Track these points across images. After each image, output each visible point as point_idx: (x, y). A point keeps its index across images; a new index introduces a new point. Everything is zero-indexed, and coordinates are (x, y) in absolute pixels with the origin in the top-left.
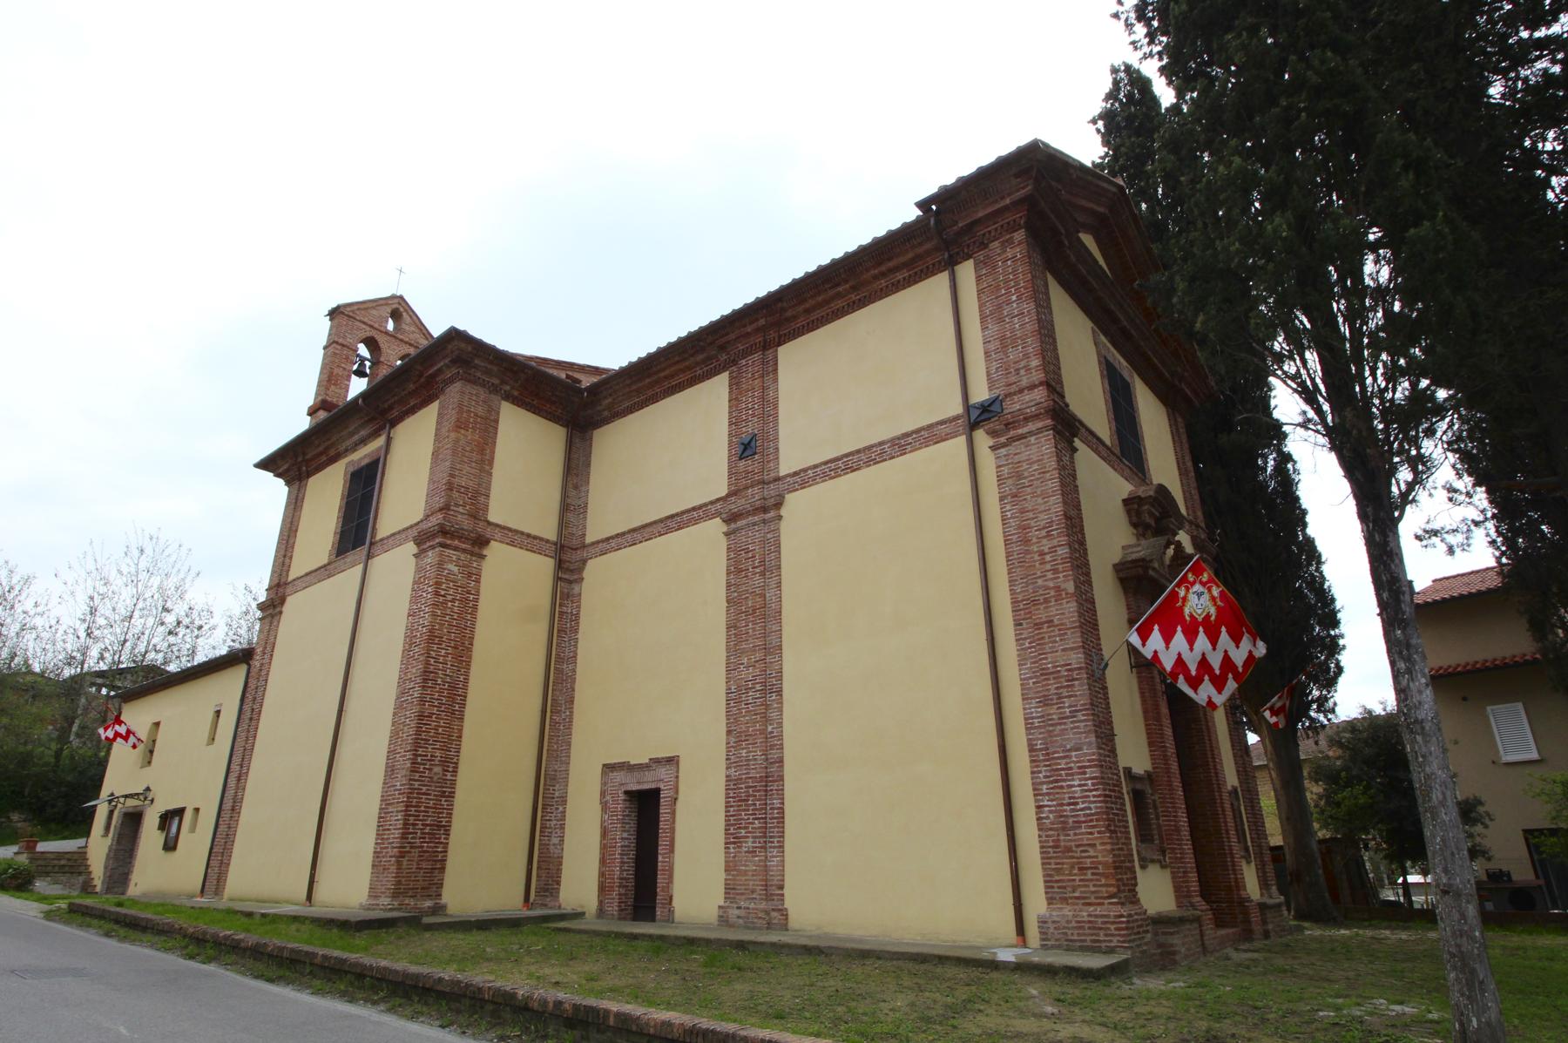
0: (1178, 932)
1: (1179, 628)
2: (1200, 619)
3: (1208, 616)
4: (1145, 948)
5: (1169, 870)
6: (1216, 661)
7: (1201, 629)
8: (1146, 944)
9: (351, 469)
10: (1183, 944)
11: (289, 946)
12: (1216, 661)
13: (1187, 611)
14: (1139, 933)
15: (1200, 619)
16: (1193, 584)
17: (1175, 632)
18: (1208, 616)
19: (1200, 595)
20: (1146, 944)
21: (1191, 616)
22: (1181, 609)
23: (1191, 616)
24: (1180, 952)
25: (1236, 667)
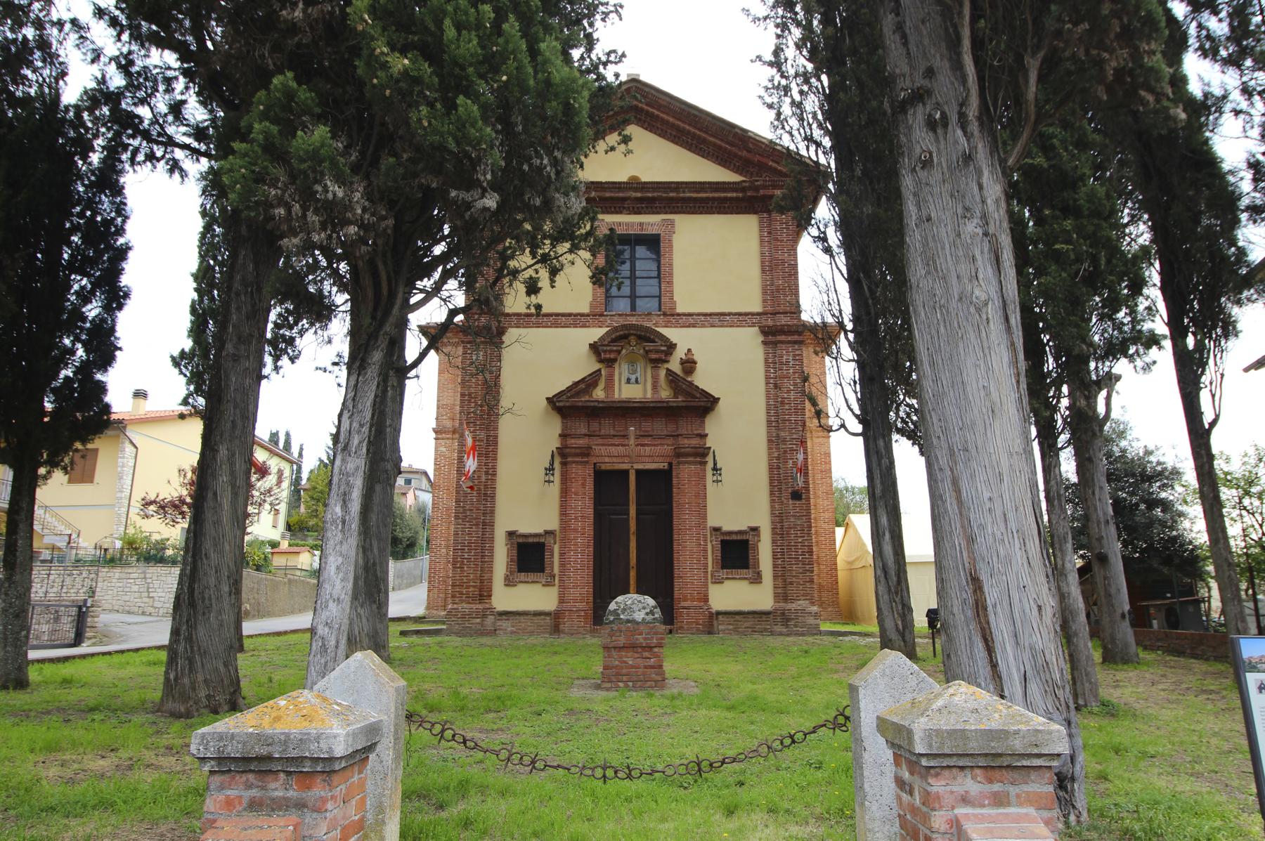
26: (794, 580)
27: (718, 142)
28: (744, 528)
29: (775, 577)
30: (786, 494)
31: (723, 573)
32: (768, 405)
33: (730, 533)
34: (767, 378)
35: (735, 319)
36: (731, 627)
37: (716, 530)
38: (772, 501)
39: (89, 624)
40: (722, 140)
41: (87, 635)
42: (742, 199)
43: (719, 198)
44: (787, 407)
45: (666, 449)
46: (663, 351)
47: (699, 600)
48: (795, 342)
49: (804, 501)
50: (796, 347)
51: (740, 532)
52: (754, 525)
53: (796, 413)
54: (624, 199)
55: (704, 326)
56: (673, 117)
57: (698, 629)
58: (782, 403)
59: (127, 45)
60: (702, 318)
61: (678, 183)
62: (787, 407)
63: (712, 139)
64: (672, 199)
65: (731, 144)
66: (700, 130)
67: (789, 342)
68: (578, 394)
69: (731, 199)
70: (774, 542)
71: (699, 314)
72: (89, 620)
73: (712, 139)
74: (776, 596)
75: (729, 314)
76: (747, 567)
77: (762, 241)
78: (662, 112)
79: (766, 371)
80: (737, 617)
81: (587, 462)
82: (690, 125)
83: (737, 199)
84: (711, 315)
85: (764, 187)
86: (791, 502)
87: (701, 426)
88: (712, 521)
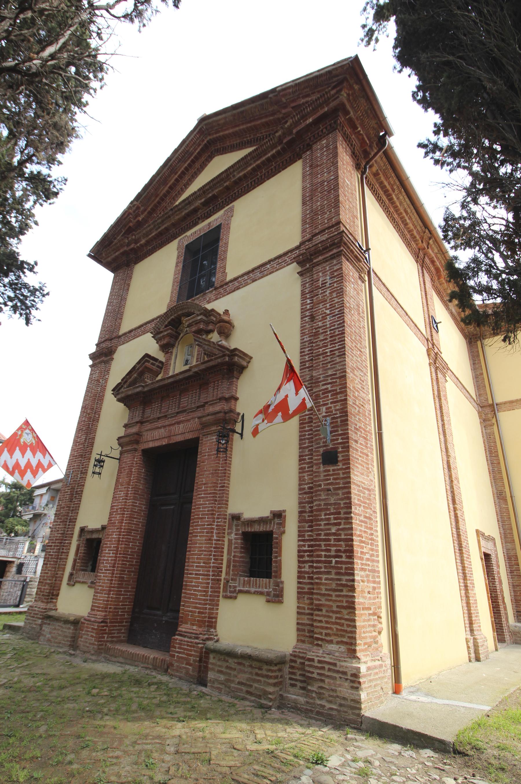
0: (49, 624)
1: (18, 448)
2: (29, 444)
3: (32, 443)
4: (34, 626)
5: (93, 591)
6: (34, 463)
7: (29, 448)
8: (36, 624)
9: (186, 243)
10: (50, 633)
11: (506, 695)
12: (34, 463)
13: (22, 440)
14: (33, 617)
15: (29, 444)
16: (25, 429)
17: (15, 449)
18: (32, 443)
19: (28, 434)
20: (36, 624)
21: (24, 442)
22: (19, 440)
23: (24, 442)
24: (45, 636)
25: (32, 467)
26: (323, 602)
27: (264, 120)
28: (266, 513)
29: (300, 594)
30: (317, 458)
31: (239, 584)
32: (302, 343)
33: (251, 522)
34: (303, 311)
35: (274, 264)
36: (222, 678)
37: (236, 517)
38: (302, 470)
39: (28, 593)
40: (266, 116)
41: (26, 599)
42: (283, 149)
43: (263, 163)
44: (321, 337)
45: (195, 424)
46: (201, 321)
47: (201, 623)
48: (333, 257)
49: (340, 465)
50: (335, 262)
51: (262, 521)
52: (277, 508)
53: (333, 342)
54: (195, 210)
55: (247, 284)
56: (233, 127)
57: (187, 673)
58: (316, 334)
59: (463, 313)
60: (246, 277)
61: (226, 171)
62: (321, 337)
63: (259, 122)
64: (227, 188)
65: (273, 114)
66: (250, 122)
67: (326, 260)
68: (133, 383)
69: (273, 156)
70: (301, 533)
71: (243, 275)
72: (28, 590)
73: (259, 122)
74: (300, 628)
75: (270, 262)
76: (268, 576)
77: (304, 177)
78: (225, 130)
79: (302, 305)
80: (232, 662)
81: (136, 450)
82: (243, 124)
83: (278, 153)
84: (253, 270)
85: (296, 124)
86: (322, 469)
87: (229, 389)
88: (233, 508)
